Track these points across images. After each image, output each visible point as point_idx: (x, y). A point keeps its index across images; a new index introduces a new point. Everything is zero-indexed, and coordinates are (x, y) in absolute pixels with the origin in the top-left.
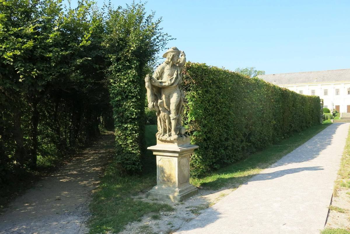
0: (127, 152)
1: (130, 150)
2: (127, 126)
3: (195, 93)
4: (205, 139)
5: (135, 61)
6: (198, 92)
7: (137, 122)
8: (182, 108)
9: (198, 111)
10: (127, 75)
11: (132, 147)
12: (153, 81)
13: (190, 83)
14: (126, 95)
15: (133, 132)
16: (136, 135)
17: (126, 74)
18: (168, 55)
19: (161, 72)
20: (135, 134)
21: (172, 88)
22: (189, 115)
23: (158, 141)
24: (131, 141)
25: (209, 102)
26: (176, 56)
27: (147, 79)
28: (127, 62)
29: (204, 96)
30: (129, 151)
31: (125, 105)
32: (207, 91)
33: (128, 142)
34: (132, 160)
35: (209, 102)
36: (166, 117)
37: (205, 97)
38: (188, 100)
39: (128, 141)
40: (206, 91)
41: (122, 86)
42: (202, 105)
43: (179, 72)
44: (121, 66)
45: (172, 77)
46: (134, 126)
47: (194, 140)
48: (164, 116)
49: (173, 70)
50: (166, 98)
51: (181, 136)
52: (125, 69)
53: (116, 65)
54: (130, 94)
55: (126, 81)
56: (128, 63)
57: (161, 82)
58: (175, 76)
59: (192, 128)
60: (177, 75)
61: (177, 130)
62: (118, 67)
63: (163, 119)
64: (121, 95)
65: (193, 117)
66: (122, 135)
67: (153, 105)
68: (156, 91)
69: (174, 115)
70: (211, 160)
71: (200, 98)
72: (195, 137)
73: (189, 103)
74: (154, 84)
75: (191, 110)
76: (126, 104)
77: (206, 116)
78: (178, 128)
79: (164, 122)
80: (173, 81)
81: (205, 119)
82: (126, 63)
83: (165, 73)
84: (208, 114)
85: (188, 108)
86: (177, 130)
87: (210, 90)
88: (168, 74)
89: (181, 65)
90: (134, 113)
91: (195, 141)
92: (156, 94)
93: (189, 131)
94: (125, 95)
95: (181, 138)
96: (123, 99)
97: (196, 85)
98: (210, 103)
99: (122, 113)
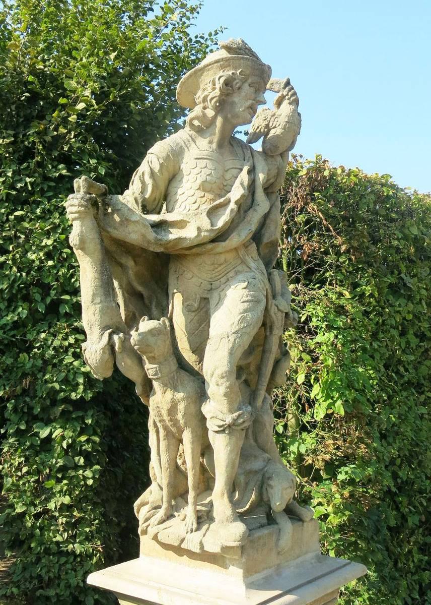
0: (47, 551)
1: (59, 538)
2: (51, 434)
3: (347, 295)
4: (389, 491)
5: (93, 162)
6: (358, 289)
7: (92, 416)
8: (277, 363)
9: (360, 370)
10: (57, 215)
11: (69, 526)
12: (117, 218)
13: (326, 253)
14: (48, 300)
15: (77, 459)
16: (88, 473)
17: (50, 212)
18: (202, 87)
19: (166, 176)
20: (84, 468)
21: (222, 258)
22: (316, 389)
23: (145, 542)
24: (67, 500)
25: (403, 334)
26: (246, 85)
27: (76, 202)
28: (61, 166)
29: (383, 308)
30: (58, 543)
31: (44, 346)
32: (394, 289)
33: (51, 506)
34: (68, 586)
35: (403, 334)
36: (180, 416)
37: (389, 314)
38: (314, 322)
39: (53, 501)
40: (391, 286)
41: (33, 261)
42: (375, 345)
43: (261, 177)
44: (32, 180)
45: (222, 200)
46: (80, 434)
47: (343, 504)
48: (172, 410)
49: (229, 164)
50: (188, 308)
51: (271, 520)
52: (51, 194)
53: (10, 174)
54: (67, 297)
55: (50, 242)
56: (63, 169)
57: (159, 226)
58: (237, 193)
59: (331, 449)
60: (252, 187)
61: (247, 484)
62: (19, 185)
63: (166, 428)
64: (27, 298)
65: (339, 402)
66: (28, 473)
67: (111, 345)
68: (138, 276)
69: (225, 410)
70: (416, 577)
71: (366, 313)
72: (346, 493)
73: (319, 338)
74: (118, 234)
75: (327, 366)
76: (46, 340)
77: (394, 391)
78: (249, 473)
79: (173, 441)
80: (222, 220)
81: (389, 404)
82: (55, 167)
83: (185, 180)
84: (402, 385)
85: (315, 360)
86: (247, 484)
87: (410, 282)
88: (199, 182)
89: (276, 147)
90: (81, 380)
91: (346, 508)
92: (140, 288)
93: (319, 465)
94: (43, 299)
95: (265, 531)
96: (35, 318)
97: (350, 260)
98: (411, 336)
99: (29, 379)
